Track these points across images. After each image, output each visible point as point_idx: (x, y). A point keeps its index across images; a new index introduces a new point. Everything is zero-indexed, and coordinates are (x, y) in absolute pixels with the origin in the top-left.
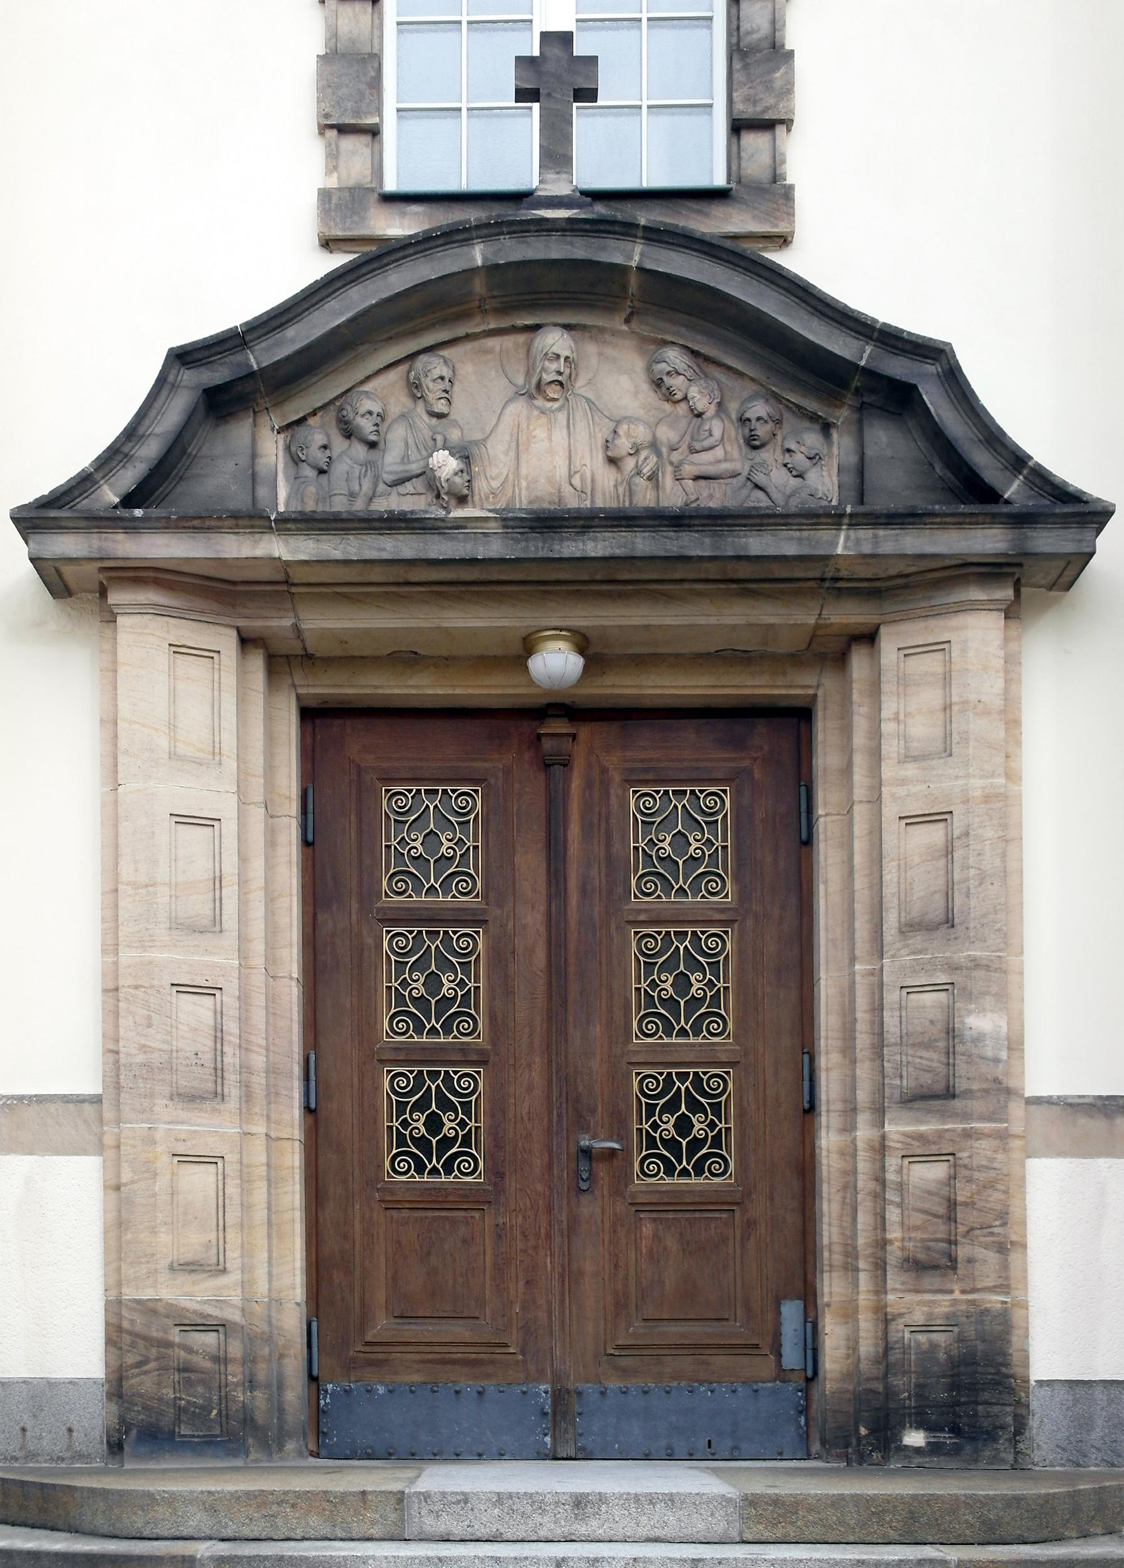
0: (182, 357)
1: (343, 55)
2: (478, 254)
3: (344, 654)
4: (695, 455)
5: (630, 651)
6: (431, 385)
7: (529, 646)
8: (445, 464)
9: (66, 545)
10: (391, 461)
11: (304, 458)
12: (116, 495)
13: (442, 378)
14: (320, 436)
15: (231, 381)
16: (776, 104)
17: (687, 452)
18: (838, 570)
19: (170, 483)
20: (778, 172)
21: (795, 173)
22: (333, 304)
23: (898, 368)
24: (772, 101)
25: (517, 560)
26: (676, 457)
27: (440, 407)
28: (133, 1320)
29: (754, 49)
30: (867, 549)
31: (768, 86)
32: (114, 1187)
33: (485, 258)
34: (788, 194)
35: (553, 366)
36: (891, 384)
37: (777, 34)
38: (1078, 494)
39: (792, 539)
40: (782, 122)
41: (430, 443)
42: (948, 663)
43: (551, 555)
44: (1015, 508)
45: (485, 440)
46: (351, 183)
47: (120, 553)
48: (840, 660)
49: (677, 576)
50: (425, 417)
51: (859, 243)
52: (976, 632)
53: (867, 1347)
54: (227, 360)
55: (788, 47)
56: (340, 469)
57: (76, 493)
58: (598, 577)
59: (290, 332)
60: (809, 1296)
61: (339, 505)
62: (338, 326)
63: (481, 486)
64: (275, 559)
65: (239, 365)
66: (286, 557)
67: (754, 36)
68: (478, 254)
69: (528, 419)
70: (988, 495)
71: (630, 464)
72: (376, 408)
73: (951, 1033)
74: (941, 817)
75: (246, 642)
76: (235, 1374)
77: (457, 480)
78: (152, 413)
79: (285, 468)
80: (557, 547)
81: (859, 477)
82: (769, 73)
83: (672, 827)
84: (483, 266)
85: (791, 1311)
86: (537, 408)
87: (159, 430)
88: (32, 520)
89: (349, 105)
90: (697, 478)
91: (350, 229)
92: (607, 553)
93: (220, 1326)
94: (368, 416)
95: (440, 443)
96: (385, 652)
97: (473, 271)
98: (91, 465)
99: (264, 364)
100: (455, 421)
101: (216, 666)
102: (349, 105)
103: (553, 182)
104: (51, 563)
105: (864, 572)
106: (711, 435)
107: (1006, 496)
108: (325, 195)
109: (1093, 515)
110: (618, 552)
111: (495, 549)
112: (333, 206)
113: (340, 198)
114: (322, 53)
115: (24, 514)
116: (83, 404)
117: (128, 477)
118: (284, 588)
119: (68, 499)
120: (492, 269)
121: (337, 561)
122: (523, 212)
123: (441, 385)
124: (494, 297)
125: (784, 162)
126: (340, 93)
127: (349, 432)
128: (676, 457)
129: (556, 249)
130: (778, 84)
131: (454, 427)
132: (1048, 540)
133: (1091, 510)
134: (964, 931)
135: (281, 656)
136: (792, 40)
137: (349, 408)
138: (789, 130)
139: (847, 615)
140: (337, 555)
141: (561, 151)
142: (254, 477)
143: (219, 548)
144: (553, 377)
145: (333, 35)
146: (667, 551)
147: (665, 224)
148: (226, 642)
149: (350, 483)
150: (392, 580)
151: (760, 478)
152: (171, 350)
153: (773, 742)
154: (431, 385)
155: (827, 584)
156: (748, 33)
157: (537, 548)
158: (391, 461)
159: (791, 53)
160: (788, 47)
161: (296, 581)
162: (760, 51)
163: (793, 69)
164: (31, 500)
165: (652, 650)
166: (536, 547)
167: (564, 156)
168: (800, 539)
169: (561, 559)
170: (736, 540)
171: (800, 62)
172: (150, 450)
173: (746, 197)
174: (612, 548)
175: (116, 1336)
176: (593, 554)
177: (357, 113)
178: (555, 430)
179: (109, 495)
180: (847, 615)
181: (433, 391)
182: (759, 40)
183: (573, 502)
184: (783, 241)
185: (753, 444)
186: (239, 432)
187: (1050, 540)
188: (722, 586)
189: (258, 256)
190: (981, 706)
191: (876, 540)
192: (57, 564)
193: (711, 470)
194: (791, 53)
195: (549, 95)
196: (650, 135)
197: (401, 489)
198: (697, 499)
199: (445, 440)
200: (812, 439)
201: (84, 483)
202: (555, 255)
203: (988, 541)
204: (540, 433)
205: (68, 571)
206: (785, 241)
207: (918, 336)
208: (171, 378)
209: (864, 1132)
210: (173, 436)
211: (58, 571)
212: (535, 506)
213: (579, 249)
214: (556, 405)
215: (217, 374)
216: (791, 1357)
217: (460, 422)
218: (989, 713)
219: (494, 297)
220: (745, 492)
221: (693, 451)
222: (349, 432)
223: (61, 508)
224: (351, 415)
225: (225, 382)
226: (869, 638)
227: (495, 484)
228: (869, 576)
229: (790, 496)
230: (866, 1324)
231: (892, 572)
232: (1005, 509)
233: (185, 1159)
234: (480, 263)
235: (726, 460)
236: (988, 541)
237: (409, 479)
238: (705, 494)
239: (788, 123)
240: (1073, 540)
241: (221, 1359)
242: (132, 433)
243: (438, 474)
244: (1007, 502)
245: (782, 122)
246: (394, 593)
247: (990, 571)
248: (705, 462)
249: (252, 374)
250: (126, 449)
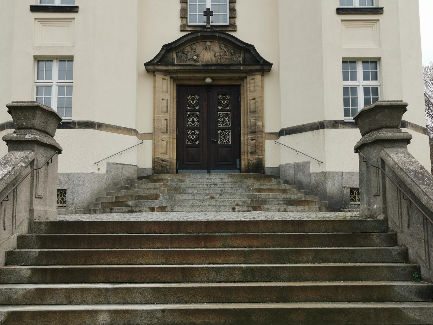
0: (164, 46)
7: (205, 78)
8: (195, 57)
9: (150, 67)
10: (189, 57)
23: (248, 47)
28: (156, 160)
31: (233, 14)
32: (154, 144)
34: (236, 26)
36: (248, 49)
48: (243, 80)
51: (243, 34)
52: (258, 78)
53: (246, 164)
60: (240, 160)
70: (259, 62)
73: (256, 125)
74: (254, 99)
75: (171, 78)
76: (168, 167)
81: (244, 59)
83: (223, 102)
85: (238, 160)
88: (146, 65)
93: (167, 161)
108: (181, 25)
109: (271, 65)
111: (201, 68)
116: (153, 51)
117: (158, 59)
127: (184, 53)
132: (265, 67)
134: (257, 113)
139: (243, 75)
145: (182, 7)
148: (168, 78)
153: (235, 91)
166: (206, 68)
175: (154, 162)
178: (208, 54)
180: (243, 75)
181: (194, 49)
185: (232, 55)
186: (171, 54)
189: (174, 34)
196: (220, 20)
200: (239, 55)
201: (153, 60)
203: (259, 67)
209: (246, 137)
216: (238, 167)
222: (184, 53)
225: (168, 49)
226: (246, 77)
230: (246, 161)
233: (163, 140)
236: (259, 67)
241: (167, 165)
242: (158, 55)
247: (259, 71)
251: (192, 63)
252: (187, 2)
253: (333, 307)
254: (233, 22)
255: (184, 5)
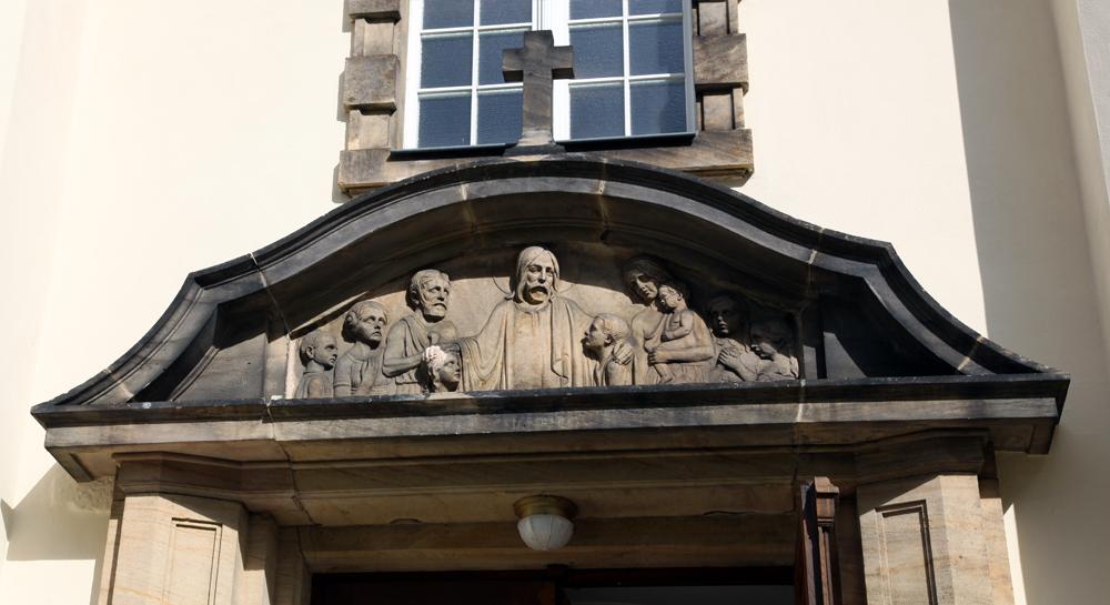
0: (202, 279)
1: (367, 57)
2: (463, 191)
3: (347, 523)
4: (668, 343)
5: (622, 515)
6: (428, 294)
8: (438, 357)
10: (392, 355)
11: (312, 356)
12: (131, 392)
13: (438, 289)
14: (328, 339)
15: (244, 297)
16: (732, 72)
17: (659, 341)
18: (806, 437)
19: (188, 380)
20: (737, 120)
21: (749, 121)
22: (336, 234)
24: (729, 71)
25: (493, 435)
26: (650, 345)
27: (437, 311)
29: (711, 35)
30: (825, 417)
31: (725, 60)
33: (469, 194)
34: (746, 137)
35: (536, 275)
37: (731, 24)
38: (1029, 365)
39: (752, 410)
40: (738, 85)
41: (427, 341)
42: (924, 520)
43: (524, 429)
44: (967, 379)
45: (476, 337)
46: (370, 146)
47: (129, 440)
49: (653, 446)
50: (423, 320)
54: (241, 280)
55: (741, 32)
56: (345, 364)
57: (95, 391)
58: (577, 448)
59: (299, 256)
61: (345, 392)
62: (341, 251)
63: (472, 374)
64: (269, 440)
65: (252, 283)
66: (280, 438)
67: (712, 26)
68: (463, 191)
69: (515, 318)
71: (607, 352)
72: (378, 314)
77: (447, 369)
78: (170, 324)
79: (296, 366)
80: (529, 422)
82: (724, 51)
84: (467, 201)
86: (522, 309)
87: (175, 338)
88: (51, 416)
89: (370, 91)
90: (670, 362)
91: (366, 179)
92: (577, 426)
94: (370, 321)
95: (435, 340)
96: (388, 521)
97: (461, 204)
98: (110, 368)
99: (273, 283)
100: (450, 322)
101: (218, 537)
102: (370, 91)
103: (534, 136)
104: (65, 451)
105: (829, 437)
106: (681, 325)
107: (959, 368)
108: (346, 155)
110: (587, 425)
112: (352, 163)
113: (359, 157)
114: (349, 56)
115: (44, 410)
116: (105, 315)
117: (143, 377)
118: (287, 466)
119: (86, 396)
120: (475, 202)
121: (327, 440)
122: (504, 158)
123: (437, 294)
124: (484, 224)
125: (741, 113)
126: (363, 83)
128: (650, 345)
129: (531, 185)
130: (732, 58)
131: (448, 327)
133: (1046, 378)
135: (292, 527)
136: (742, 27)
137: (354, 315)
138: (745, 92)
140: (327, 435)
141: (541, 113)
142: (263, 374)
143: (219, 432)
144: (536, 284)
146: (632, 423)
147: (624, 162)
149: (357, 372)
150: (384, 456)
151: (730, 360)
152: (191, 275)
154: (428, 294)
155: (798, 451)
156: (707, 24)
157: (511, 424)
158: (392, 355)
159: (743, 37)
160: (741, 32)
161: (297, 459)
162: (716, 36)
163: (745, 47)
164: (52, 398)
165: (639, 514)
167: (544, 117)
168: (760, 410)
169: (534, 433)
170: (699, 412)
171: (751, 45)
172: (165, 354)
173: (707, 140)
174: (580, 421)
176: (563, 428)
177: (377, 96)
178: (533, 335)
179: (124, 391)
182: (717, 29)
183: (554, 383)
184: (744, 173)
187: (1009, 406)
188: (697, 454)
189: (280, 179)
190: (962, 562)
191: (834, 411)
192: (72, 452)
193: (683, 354)
194: (743, 37)
195: (531, 75)
197: (399, 379)
198: (671, 380)
199: (440, 337)
201: (103, 381)
202: (530, 189)
204: (525, 329)
205: (85, 457)
206: (747, 171)
207: (859, 238)
208: (190, 296)
210: (187, 343)
211: (75, 458)
212: (521, 388)
213: (552, 184)
214: (540, 306)
215: (231, 292)
217: (456, 323)
218: (973, 569)
219: (484, 224)
220: (717, 372)
221: (664, 339)
223: (80, 404)
224: (355, 321)
225: (241, 301)
227: (484, 373)
228: (839, 442)
229: (759, 375)
231: (860, 438)
232: (957, 379)
234: (465, 198)
235: (698, 346)
237: (406, 371)
238: (679, 374)
239: (743, 86)
240: (1032, 406)
242: (148, 341)
243: (430, 365)
244: (961, 373)
245: (738, 85)
246: (388, 467)
248: (675, 348)
249: (263, 291)
250: (143, 354)
251: (415, 392)
252: (394, 17)
253: (408, 86)
254: (722, 20)
255: (372, 33)
